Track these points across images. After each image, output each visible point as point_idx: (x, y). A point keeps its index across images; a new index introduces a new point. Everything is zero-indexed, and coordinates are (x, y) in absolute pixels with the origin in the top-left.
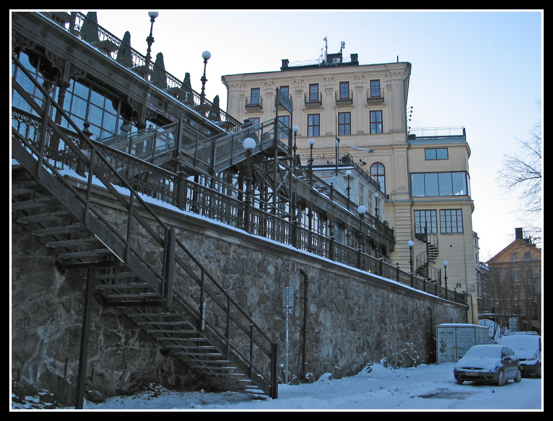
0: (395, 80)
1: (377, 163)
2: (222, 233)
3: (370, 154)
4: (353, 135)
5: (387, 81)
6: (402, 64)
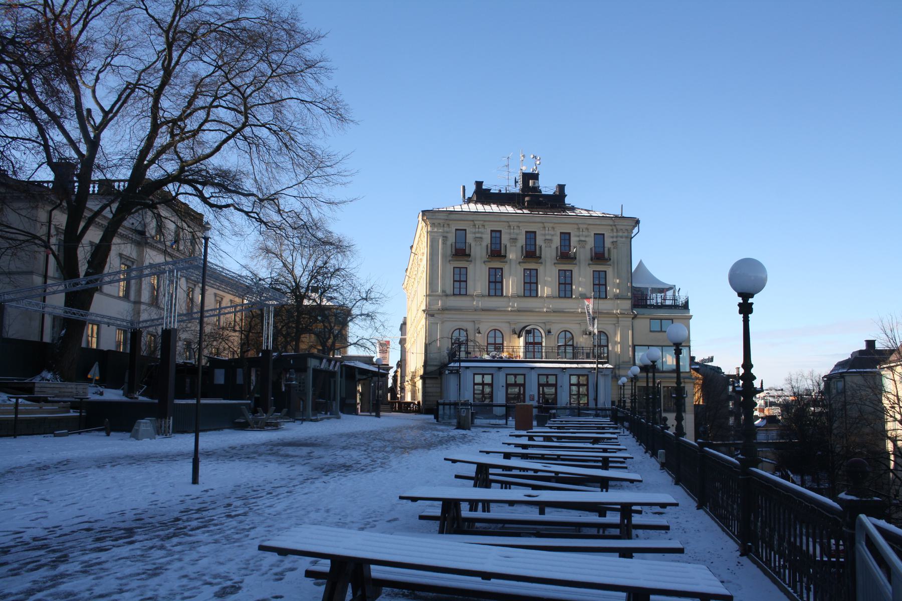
0: (622, 237)
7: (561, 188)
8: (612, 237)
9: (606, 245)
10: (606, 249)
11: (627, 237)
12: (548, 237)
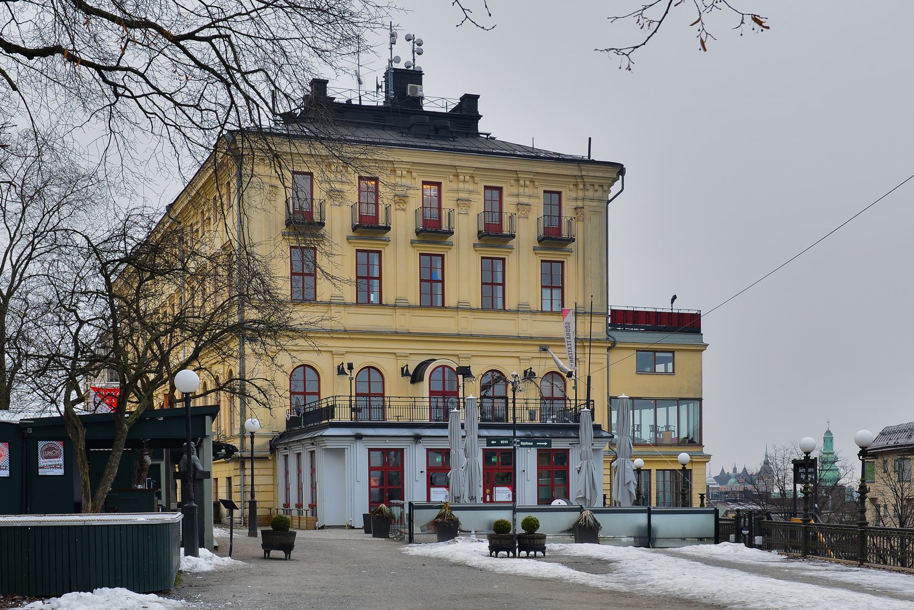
0: (592, 200)
1: (369, 367)
2: (665, 596)
3: (543, 355)
4: (387, 305)
5: (576, 199)
6: (610, 168)
7: (469, 102)
8: (576, 199)
9: (444, 204)
10: (316, 203)
11: (600, 200)
12: (463, 195)
